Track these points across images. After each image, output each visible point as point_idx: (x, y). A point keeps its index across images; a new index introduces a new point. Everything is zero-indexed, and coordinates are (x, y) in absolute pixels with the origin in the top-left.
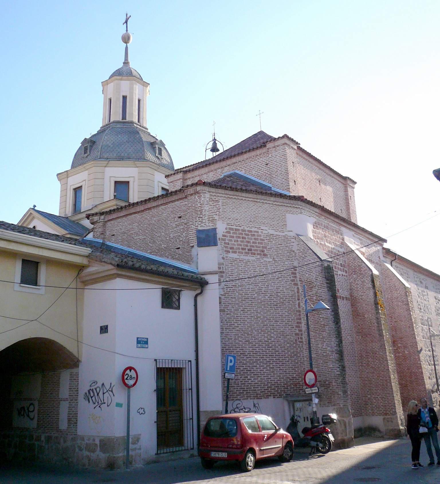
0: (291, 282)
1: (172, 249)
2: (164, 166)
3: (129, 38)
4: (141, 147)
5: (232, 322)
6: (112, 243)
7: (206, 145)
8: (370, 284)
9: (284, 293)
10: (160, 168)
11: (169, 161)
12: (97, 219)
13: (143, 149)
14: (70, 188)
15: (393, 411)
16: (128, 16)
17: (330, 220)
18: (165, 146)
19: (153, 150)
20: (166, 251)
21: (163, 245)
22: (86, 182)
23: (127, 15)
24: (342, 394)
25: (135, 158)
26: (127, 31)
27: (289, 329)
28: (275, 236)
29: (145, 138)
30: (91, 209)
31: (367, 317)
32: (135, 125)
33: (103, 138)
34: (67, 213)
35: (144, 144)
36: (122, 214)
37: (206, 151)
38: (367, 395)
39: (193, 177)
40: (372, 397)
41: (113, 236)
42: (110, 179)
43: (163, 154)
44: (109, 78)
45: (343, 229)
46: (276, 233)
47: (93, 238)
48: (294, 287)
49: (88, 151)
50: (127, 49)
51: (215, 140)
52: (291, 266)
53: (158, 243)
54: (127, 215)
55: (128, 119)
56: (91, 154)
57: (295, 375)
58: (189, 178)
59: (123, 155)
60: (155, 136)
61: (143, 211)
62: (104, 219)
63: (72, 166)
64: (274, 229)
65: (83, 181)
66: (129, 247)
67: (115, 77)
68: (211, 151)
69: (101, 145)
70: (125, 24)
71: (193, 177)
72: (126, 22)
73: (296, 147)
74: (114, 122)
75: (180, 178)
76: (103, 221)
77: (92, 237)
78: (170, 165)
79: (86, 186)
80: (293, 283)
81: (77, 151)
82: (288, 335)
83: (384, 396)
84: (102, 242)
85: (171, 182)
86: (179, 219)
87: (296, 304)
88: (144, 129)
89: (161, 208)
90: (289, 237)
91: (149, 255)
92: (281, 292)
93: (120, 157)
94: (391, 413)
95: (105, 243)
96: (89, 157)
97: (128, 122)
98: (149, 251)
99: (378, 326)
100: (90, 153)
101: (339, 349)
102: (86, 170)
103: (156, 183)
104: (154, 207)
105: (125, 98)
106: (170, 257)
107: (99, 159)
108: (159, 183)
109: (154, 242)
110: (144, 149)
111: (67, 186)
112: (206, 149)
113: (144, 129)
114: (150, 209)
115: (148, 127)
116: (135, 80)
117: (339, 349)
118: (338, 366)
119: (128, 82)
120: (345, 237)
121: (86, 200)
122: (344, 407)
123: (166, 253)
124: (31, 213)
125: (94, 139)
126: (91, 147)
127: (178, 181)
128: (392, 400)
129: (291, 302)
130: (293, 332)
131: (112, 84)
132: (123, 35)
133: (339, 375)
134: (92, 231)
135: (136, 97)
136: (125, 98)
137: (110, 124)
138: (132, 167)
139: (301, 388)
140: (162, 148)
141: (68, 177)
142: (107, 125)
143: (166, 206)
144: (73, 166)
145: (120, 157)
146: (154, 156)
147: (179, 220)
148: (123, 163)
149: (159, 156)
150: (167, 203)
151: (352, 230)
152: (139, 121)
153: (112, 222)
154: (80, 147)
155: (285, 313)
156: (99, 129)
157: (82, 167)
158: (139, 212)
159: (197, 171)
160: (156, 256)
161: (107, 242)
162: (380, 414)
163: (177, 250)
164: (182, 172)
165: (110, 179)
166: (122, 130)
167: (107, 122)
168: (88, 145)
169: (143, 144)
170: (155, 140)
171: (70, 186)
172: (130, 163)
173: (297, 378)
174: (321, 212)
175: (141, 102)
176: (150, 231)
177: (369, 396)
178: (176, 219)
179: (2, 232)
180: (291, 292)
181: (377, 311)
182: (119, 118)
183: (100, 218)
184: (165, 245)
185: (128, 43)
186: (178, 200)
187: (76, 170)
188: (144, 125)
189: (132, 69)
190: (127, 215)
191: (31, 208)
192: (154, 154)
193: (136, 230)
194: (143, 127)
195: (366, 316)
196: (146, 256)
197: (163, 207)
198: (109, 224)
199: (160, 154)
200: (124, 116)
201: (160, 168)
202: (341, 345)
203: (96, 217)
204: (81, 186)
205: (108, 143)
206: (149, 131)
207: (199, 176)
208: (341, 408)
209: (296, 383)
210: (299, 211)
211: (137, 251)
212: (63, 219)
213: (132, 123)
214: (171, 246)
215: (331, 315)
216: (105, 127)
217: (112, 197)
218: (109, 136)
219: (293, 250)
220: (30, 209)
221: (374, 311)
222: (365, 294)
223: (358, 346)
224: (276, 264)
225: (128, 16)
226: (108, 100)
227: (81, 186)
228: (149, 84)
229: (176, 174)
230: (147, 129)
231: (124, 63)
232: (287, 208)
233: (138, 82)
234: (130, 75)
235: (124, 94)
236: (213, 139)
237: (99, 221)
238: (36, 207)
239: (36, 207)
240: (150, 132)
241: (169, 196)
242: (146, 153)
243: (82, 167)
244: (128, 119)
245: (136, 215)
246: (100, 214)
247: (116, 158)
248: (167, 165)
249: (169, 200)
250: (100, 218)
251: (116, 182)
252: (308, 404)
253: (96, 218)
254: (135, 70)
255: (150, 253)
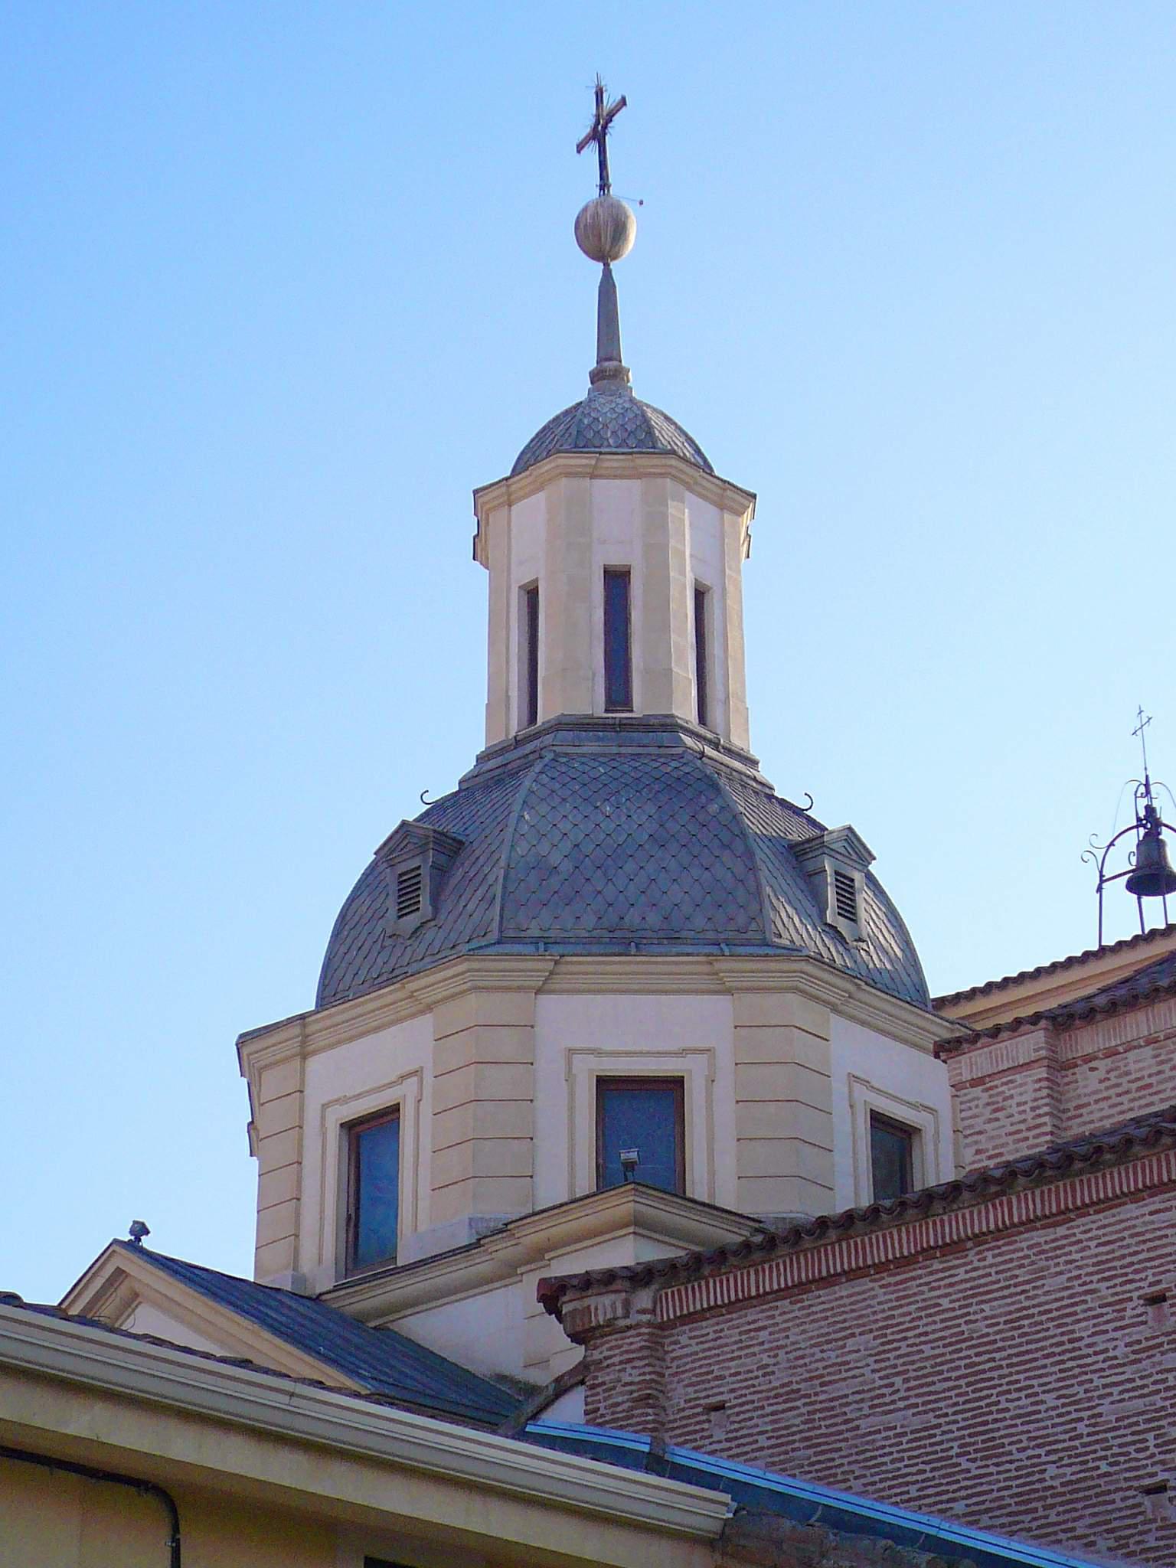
1: (1117, 1496)
2: (872, 980)
3: (619, 230)
4: (739, 868)
6: (712, 1453)
7: (1100, 854)
10: (860, 995)
11: (899, 953)
12: (614, 1309)
13: (751, 883)
14: (323, 1118)
16: (609, 102)
18: (873, 868)
19: (803, 886)
20: (1079, 1505)
21: (1052, 1470)
22: (421, 1082)
23: (599, 94)
25: (710, 935)
26: (604, 185)
29: (756, 822)
30: (468, 1248)
32: (688, 741)
33: (512, 821)
34: (307, 1266)
35: (758, 851)
36: (772, 1279)
37: (1100, 889)
39: (1111, 1053)
41: (713, 1416)
42: (569, 1064)
43: (862, 915)
44: (515, 472)
47: (588, 1423)
49: (424, 899)
50: (607, 292)
51: (1151, 822)
53: (1017, 1456)
54: (802, 1287)
55: (641, 705)
56: (442, 916)
58: (1088, 1059)
59: (632, 918)
60: (801, 803)
61: (904, 1262)
62: (653, 1312)
63: (324, 985)
65: (403, 1077)
66: (830, 1480)
67: (562, 460)
68: (1131, 887)
69: (502, 863)
70: (592, 151)
71: (1111, 1053)
72: (598, 135)
74: (560, 725)
75: (1034, 1056)
76: (649, 1324)
77: (582, 1419)
78: (906, 979)
79: (427, 1108)
81: (351, 900)
84: (646, 1449)
85: (976, 1082)
86: (1149, 1309)
88: (737, 765)
89: (1025, 1241)
91: (966, 1531)
93: (618, 934)
95: (667, 1457)
96: (429, 934)
97: (645, 725)
98: (959, 1507)
100: (436, 910)
102: (422, 1012)
103: (839, 1086)
104: (979, 1239)
105: (617, 581)
106: (1102, 1544)
107: (498, 943)
108: (856, 1086)
109: (992, 1452)
110: (759, 886)
111: (302, 1110)
112: (1102, 881)
113: (737, 765)
114: (953, 1248)
115: (754, 752)
116: (674, 478)
119: (634, 487)
121: (424, 1190)
123: (1074, 1520)
124: (119, 1272)
125: (453, 829)
126: (441, 873)
127: (1018, 1078)
131: (539, 499)
132: (585, 210)
134: (582, 1382)
135: (683, 573)
136: (617, 581)
137: (537, 736)
138: (697, 992)
140: (858, 877)
141: (304, 1057)
142: (518, 742)
143: (1061, 1231)
144: (331, 991)
145: (618, 934)
146: (815, 928)
147: (1149, 1318)
148: (591, 968)
149: (842, 925)
150: (1063, 1216)
152: (702, 719)
153: (708, 1327)
154: (366, 875)
156: (468, 765)
157: (400, 995)
158: (881, 1268)
159: (1141, 1016)
160: (1012, 1534)
161: (678, 1450)
163: (1147, 1501)
164: (1043, 1023)
165: (569, 1064)
166: (616, 774)
167: (514, 725)
168: (424, 864)
169: (750, 854)
170: (811, 833)
171: (324, 1107)
172: (689, 965)
175: (713, 605)
176: (962, 1382)
178: (1129, 1313)
179: (292, 1395)
182: (591, 701)
183: (627, 1304)
184: (1068, 1470)
185: (614, 258)
186: (1135, 1196)
187: (359, 1010)
188: (737, 742)
189: (649, 413)
190: (802, 1287)
191: (116, 1242)
192: (814, 912)
193: (869, 1376)
194: (729, 752)
196: (943, 1535)
197: (1039, 1237)
198: (684, 1340)
199: (848, 910)
200: (618, 690)
201: (860, 995)
203: (606, 1300)
204: (395, 1109)
205: (544, 848)
206: (765, 773)
207: (1151, 1041)
211: (878, 1506)
212: (294, 1304)
213: (669, 725)
214: (1107, 1474)
216: (510, 756)
217: (586, 1181)
218: (543, 809)
220: (115, 1247)
225: (609, 102)
226: (515, 591)
227: (395, 1109)
228: (754, 496)
229: (1004, 1035)
230: (754, 763)
231: (596, 376)
233: (690, 489)
234: (640, 443)
235: (616, 560)
236: (1142, 814)
237: (622, 1323)
238: (147, 1232)
239: (147, 1232)
240: (771, 781)
241: (1081, 1172)
242: (774, 909)
243: (400, 995)
244: (641, 705)
245: (865, 1284)
246: (631, 1279)
247: (598, 941)
248: (888, 981)
249: (1083, 1196)
250: (627, 1304)
251: (605, 1085)
253: (603, 1306)
254: (667, 418)
255: (971, 1519)
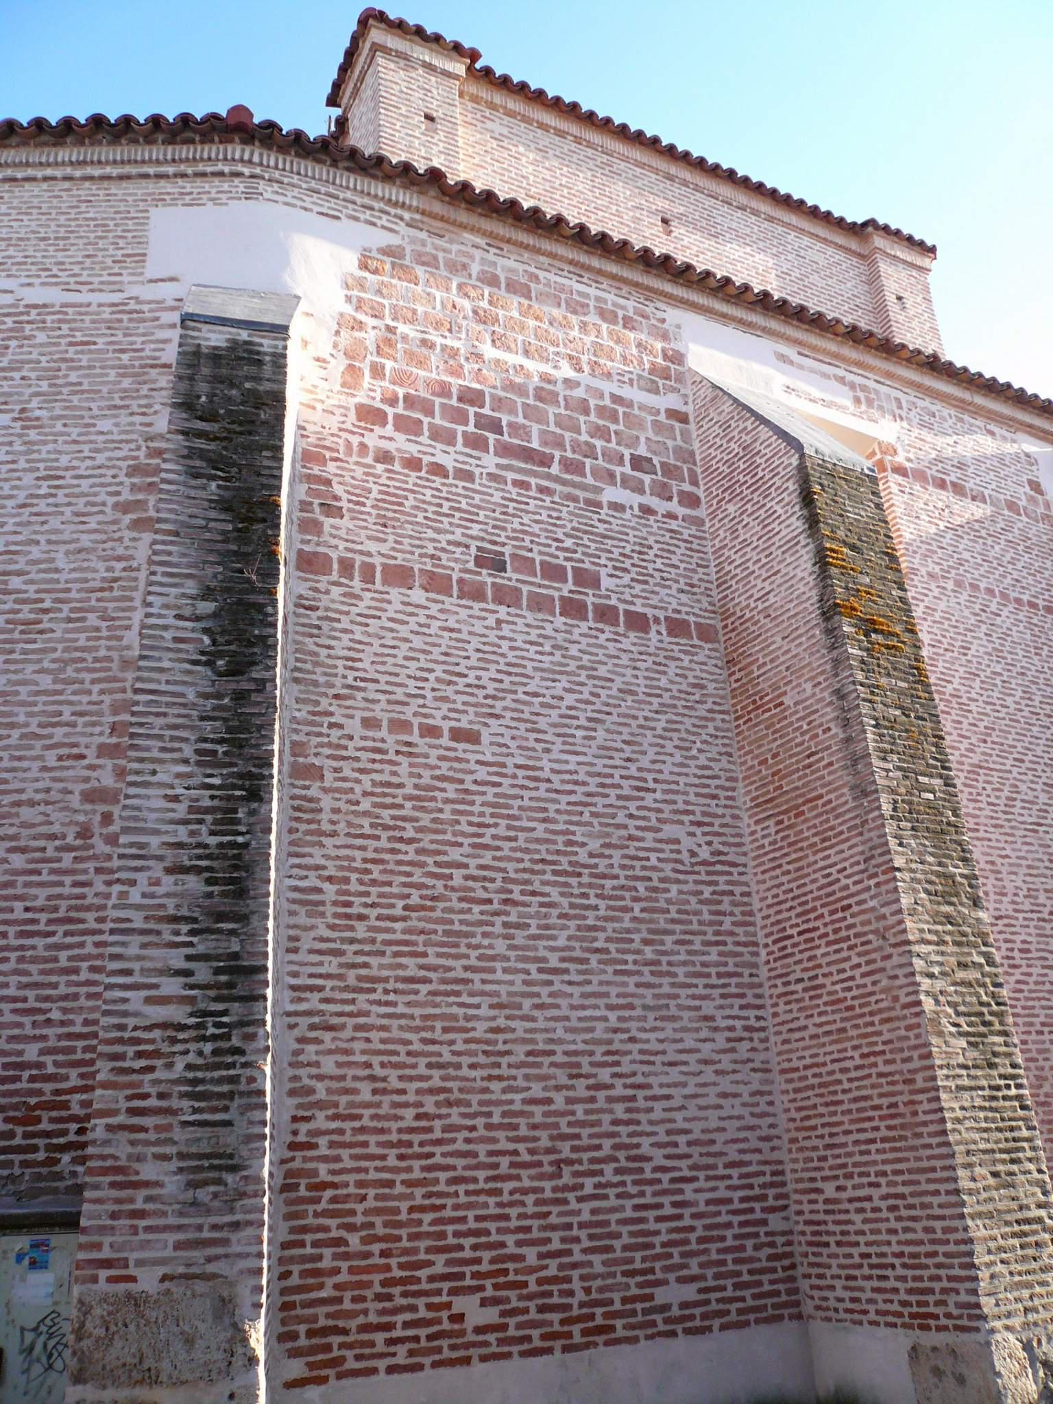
0: (119, 515)
5: (643, 910)
8: (794, 519)
9: (57, 570)
15: (964, 1297)
17: (542, 259)
24: (172, 1185)
27: (44, 769)
28: (57, 308)
31: (796, 704)
38: (819, 1185)
40: (844, 1195)
45: (673, 315)
46: (54, 296)
48: (134, 539)
52: (134, 437)
57: (31, 1052)
64: (56, 284)
73: (459, 68)
80: (127, 519)
82: (32, 803)
83: (906, 1190)
87: (128, 628)
90: (145, 307)
92: (28, 568)
94: (948, 1316)
99: (848, 740)
101: (213, 840)
117: (213, 840)
118: (183, 965)
120: (692, 346)
122: (177, 1289)
128: (952, 1217)
129: (93, 620)
130: (70, 786)
133: (182, 1027)
139: (72, 1137)
151: (764, 329)
155: (36, 677)
162: (890, 1320)
173: (51, 1069)
174: (437, 207)
177: (829, 1190)
180: (101, 566)
181: (835, 653)
195: (788, 701)
202: (252, 813)
208: (135, 1301)
209: (33, 1101)
210: (240, 185)
215: (179, 617)
219: (163, 361)
221: (820, 661)
222: (778, 579)
223: (764, 882)
224: (33, 435)
232: (163, 183)
252: (20, 1258)
